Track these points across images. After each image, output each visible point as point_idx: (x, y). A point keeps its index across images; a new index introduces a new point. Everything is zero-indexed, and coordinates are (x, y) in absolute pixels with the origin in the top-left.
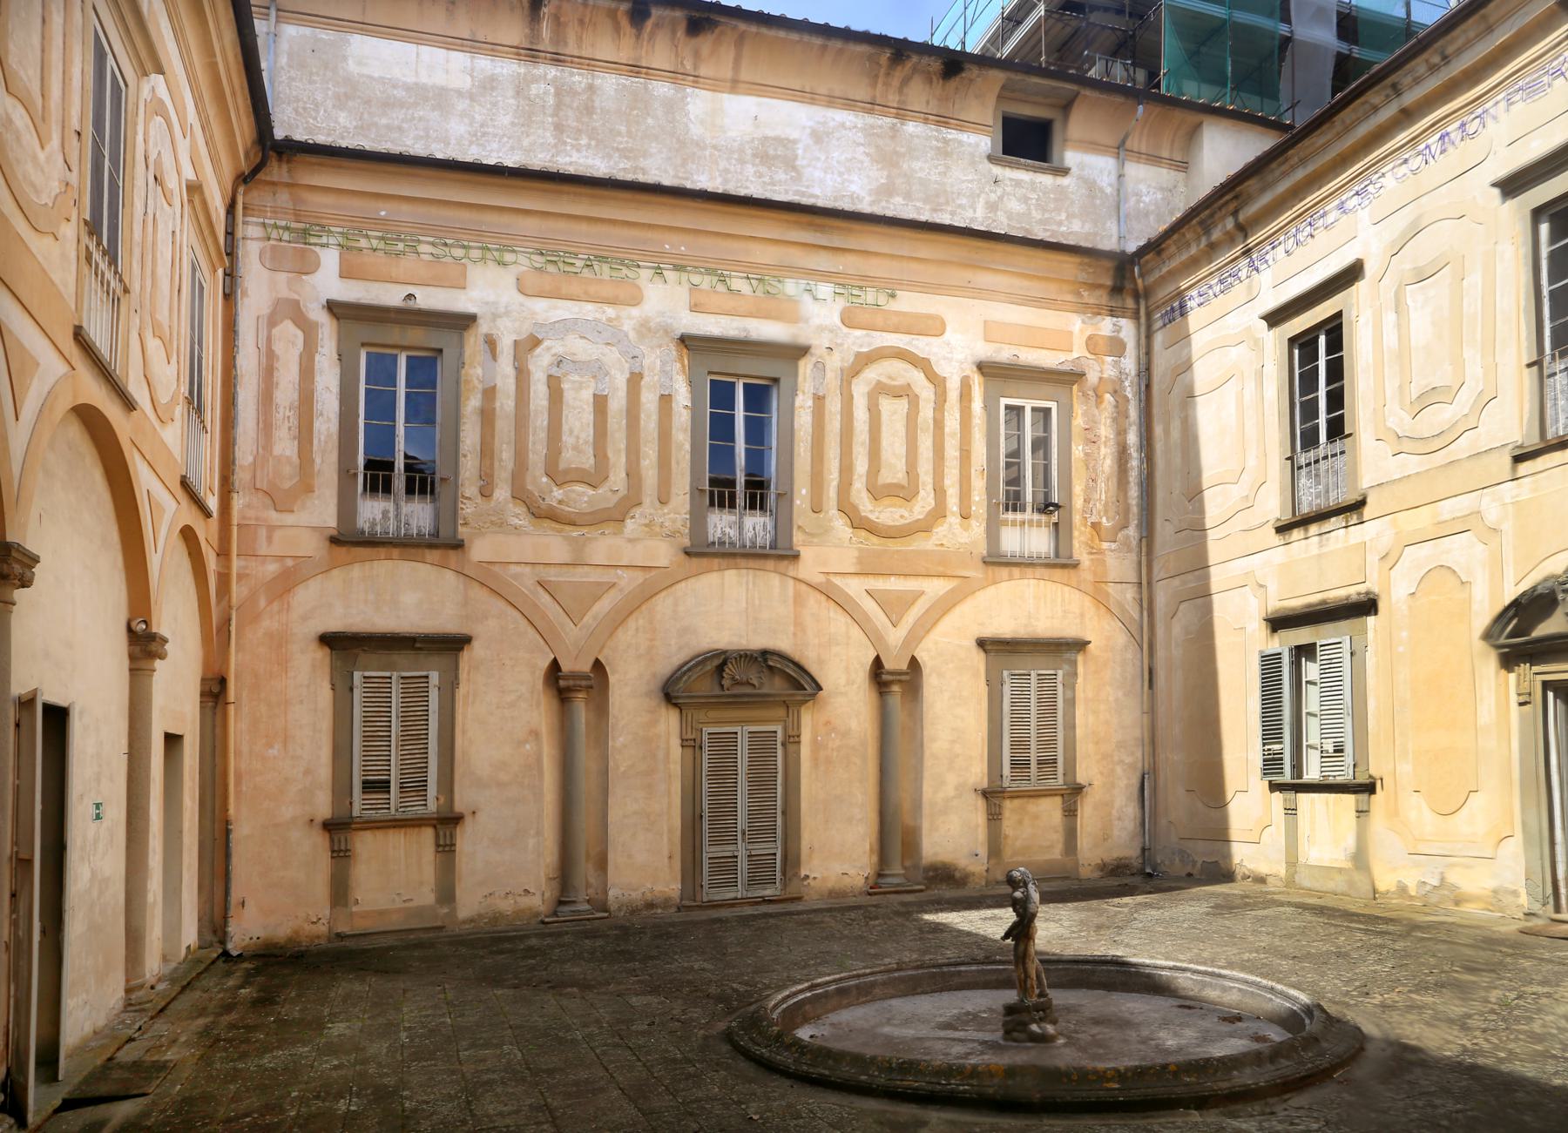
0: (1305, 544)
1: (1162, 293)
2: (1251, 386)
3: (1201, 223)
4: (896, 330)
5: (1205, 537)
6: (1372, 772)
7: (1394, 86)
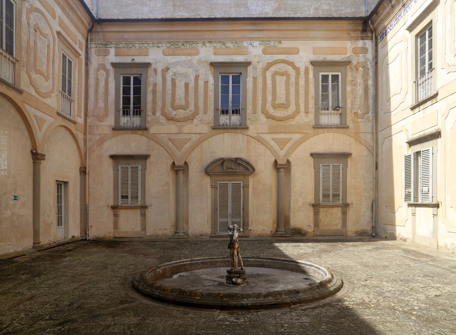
0: (420, 113)
1: (380, 29)
5: (390, 115)
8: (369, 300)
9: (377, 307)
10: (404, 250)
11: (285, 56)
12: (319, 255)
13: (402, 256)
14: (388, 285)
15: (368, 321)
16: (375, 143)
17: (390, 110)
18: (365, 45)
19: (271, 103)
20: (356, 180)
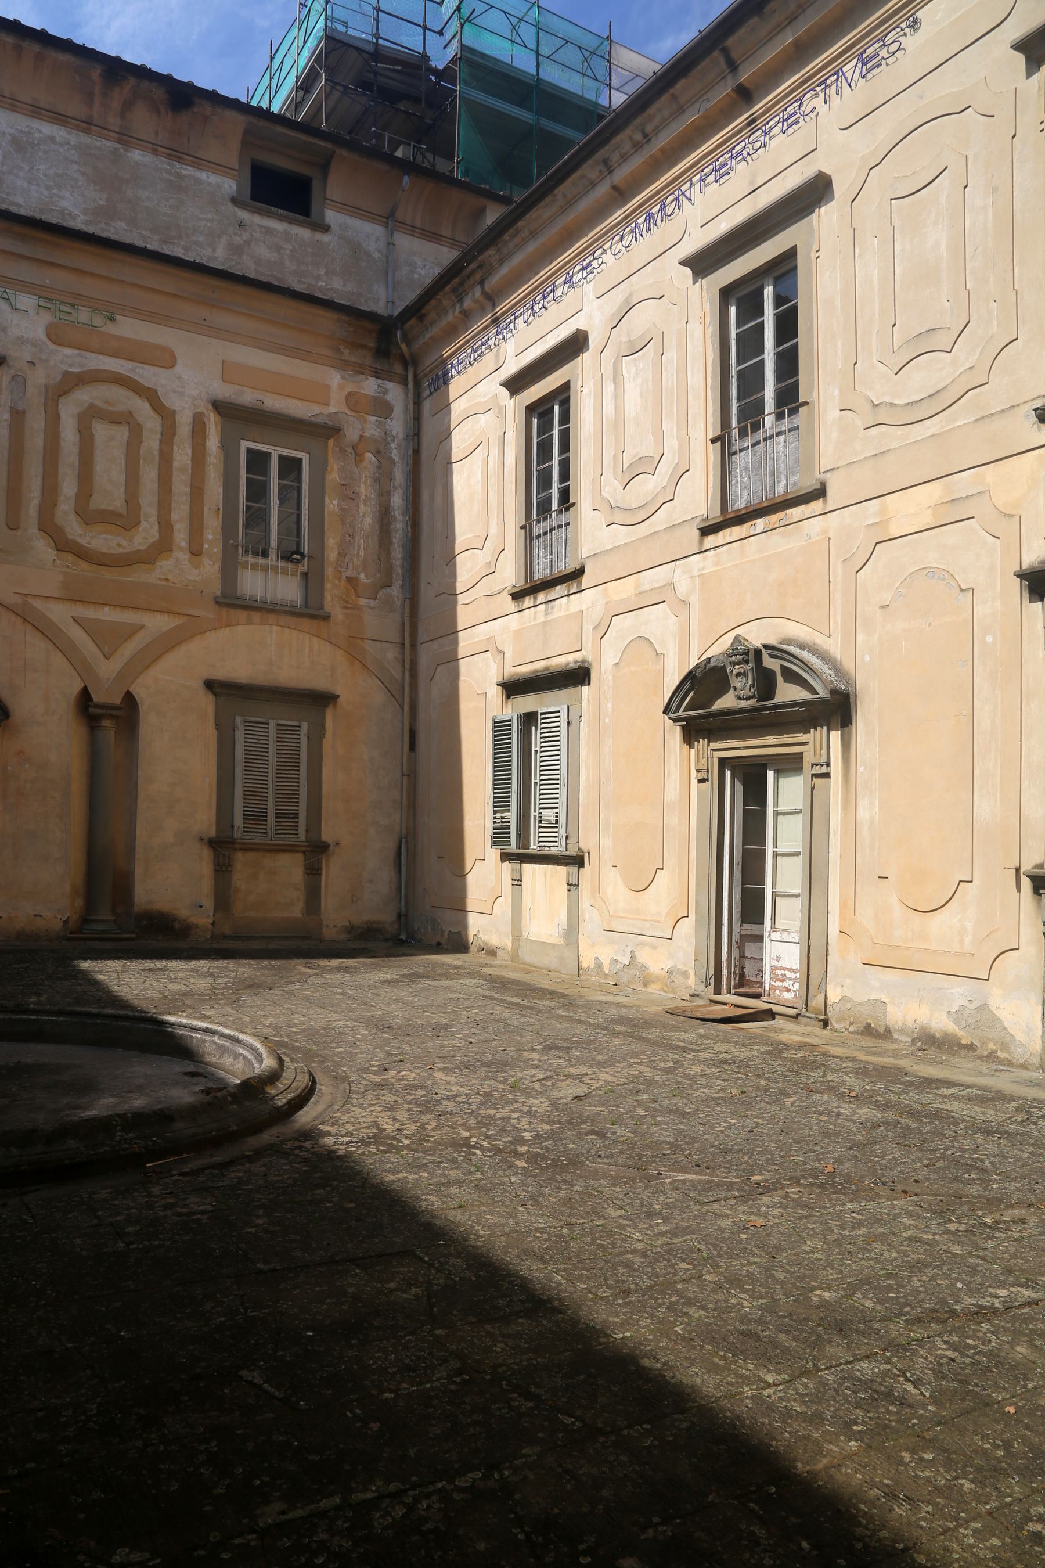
0: (535, 613)
1: (428, 361)
2: (494, 452)
3: (454, 290)
4: (115, 355)
5: (455, 603)
6: (582, 845)
7: (605, 162)
8: (397, 1126)
9: (419, 1144)
10: (491, 980)
11: (130, 365)
12: (234, 997)
13: (485, 997)
14: (448, 1079)
15: (396, 1187)
16: (407, 674)
17: (455, 588)
18: (384, 394)
19: (72, 502)
20: (351, 771)
